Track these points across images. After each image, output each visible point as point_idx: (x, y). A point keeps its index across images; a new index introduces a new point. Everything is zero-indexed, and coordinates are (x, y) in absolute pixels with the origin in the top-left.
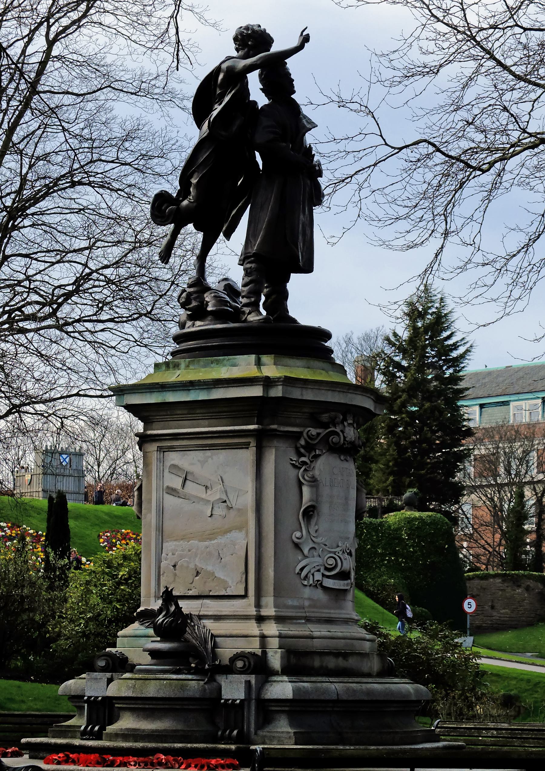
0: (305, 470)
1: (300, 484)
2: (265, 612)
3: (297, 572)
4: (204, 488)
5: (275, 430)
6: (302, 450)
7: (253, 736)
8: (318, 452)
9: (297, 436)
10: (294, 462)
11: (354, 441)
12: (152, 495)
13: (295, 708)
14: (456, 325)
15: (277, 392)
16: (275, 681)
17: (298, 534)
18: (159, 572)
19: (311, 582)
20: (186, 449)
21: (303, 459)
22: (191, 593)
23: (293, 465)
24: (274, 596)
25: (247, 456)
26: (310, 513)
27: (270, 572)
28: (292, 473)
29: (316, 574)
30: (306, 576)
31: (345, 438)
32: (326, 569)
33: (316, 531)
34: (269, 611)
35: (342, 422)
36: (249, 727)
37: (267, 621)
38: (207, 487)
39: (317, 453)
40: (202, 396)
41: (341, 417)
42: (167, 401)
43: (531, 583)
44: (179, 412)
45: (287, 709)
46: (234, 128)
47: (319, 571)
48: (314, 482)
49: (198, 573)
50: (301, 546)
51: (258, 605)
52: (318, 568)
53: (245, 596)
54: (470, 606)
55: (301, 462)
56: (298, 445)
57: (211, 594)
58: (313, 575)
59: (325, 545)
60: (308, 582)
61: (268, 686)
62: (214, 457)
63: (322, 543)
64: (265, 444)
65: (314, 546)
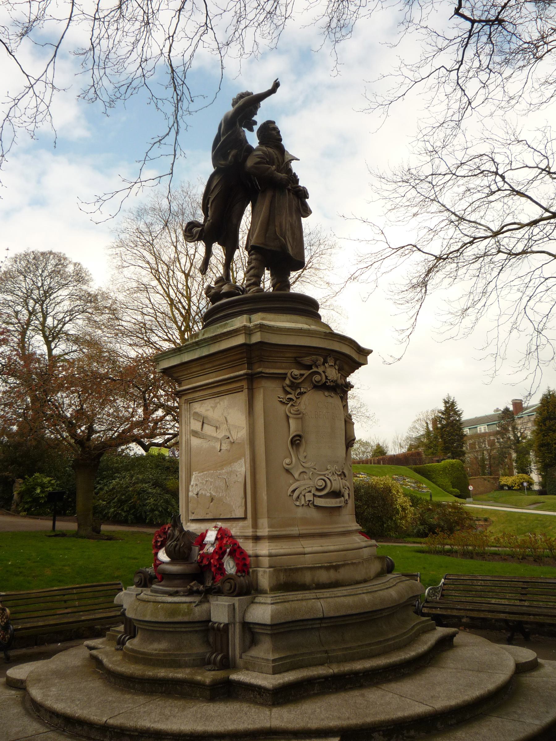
0: (292, 405)
1: (288, 417)
2: (260, 532)
3: (289, 494)
4: (215, 428)
5: (261, 372)
6: (288, 389)
7: (238, 660)
8: (302, 390)
9: (283, 377)
10: (281, 399)
11: (336, 381)
12: (183, 439)
13: (280, 630)
14: (458, 406)
15: (256, 338)
16: (260, 603)
17: (288, 461)
18: (188, 500)
19: (303, 502)
20: (203, 399)
21: (289, 396)
22: (208, 517)
23: (281, 401)
24: (268, 517)
25: (242, 397)
26: (296, 442)
27: (263, 495)
28: (283, 409)
29: (307, 494)
30: (298, 497)
31: (326, 377)
32: (317, 490)
33: (305, 457)
34: (264, 531)
35: (323, 364)
36: (234, 650)
37: (262, 541)
38: (217, 428)
39: (302, 391)
40: (205, 352)
41: (322, 360)
42: (184, 361)
43: (490, 479)
44: (195, 370)
45: (269, 632)
46: (230, 157)
47: (310, 492)
48: (300, 416)
49: (212, 500)
50: (292, 471)
51: (255, 525)
52: (308, 490)
53: (245, 518)
54: (471, 488)
55: (288, 399)
56: (284, 385)
57: (221, 517)
58: (304, 496)
59: (315, 469)
60: (301, 503)
61: (254, 606)
62: (221, 402)
63: (311, 467)
64: (255, 386)
65: (304, 470)
